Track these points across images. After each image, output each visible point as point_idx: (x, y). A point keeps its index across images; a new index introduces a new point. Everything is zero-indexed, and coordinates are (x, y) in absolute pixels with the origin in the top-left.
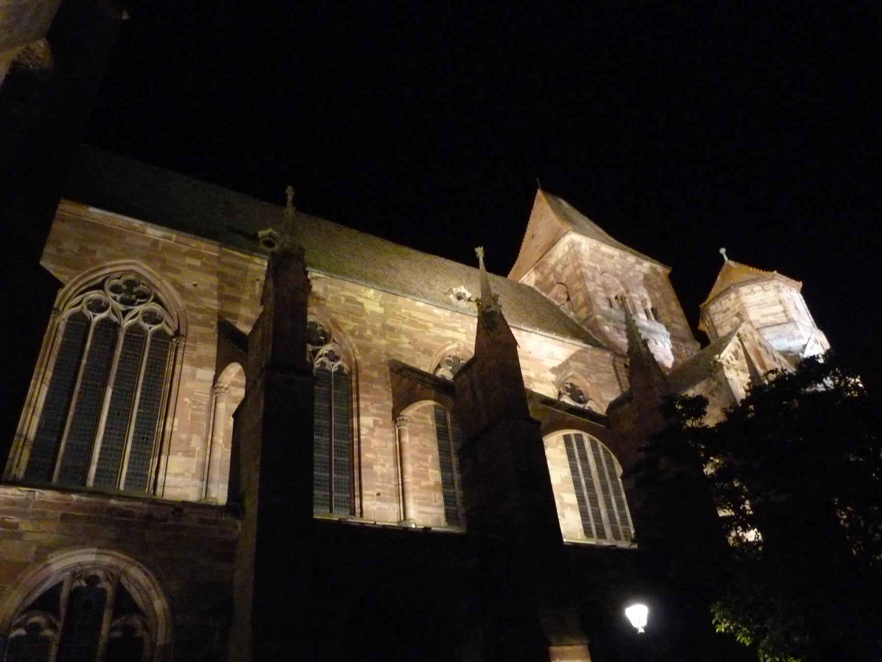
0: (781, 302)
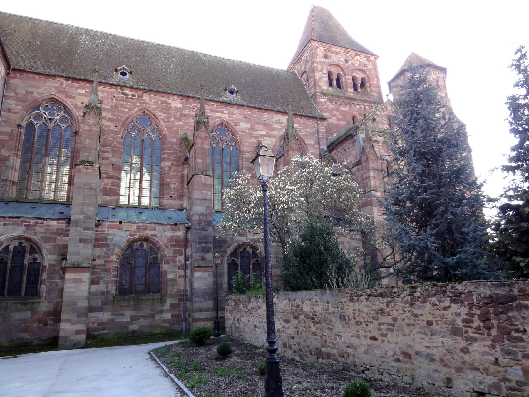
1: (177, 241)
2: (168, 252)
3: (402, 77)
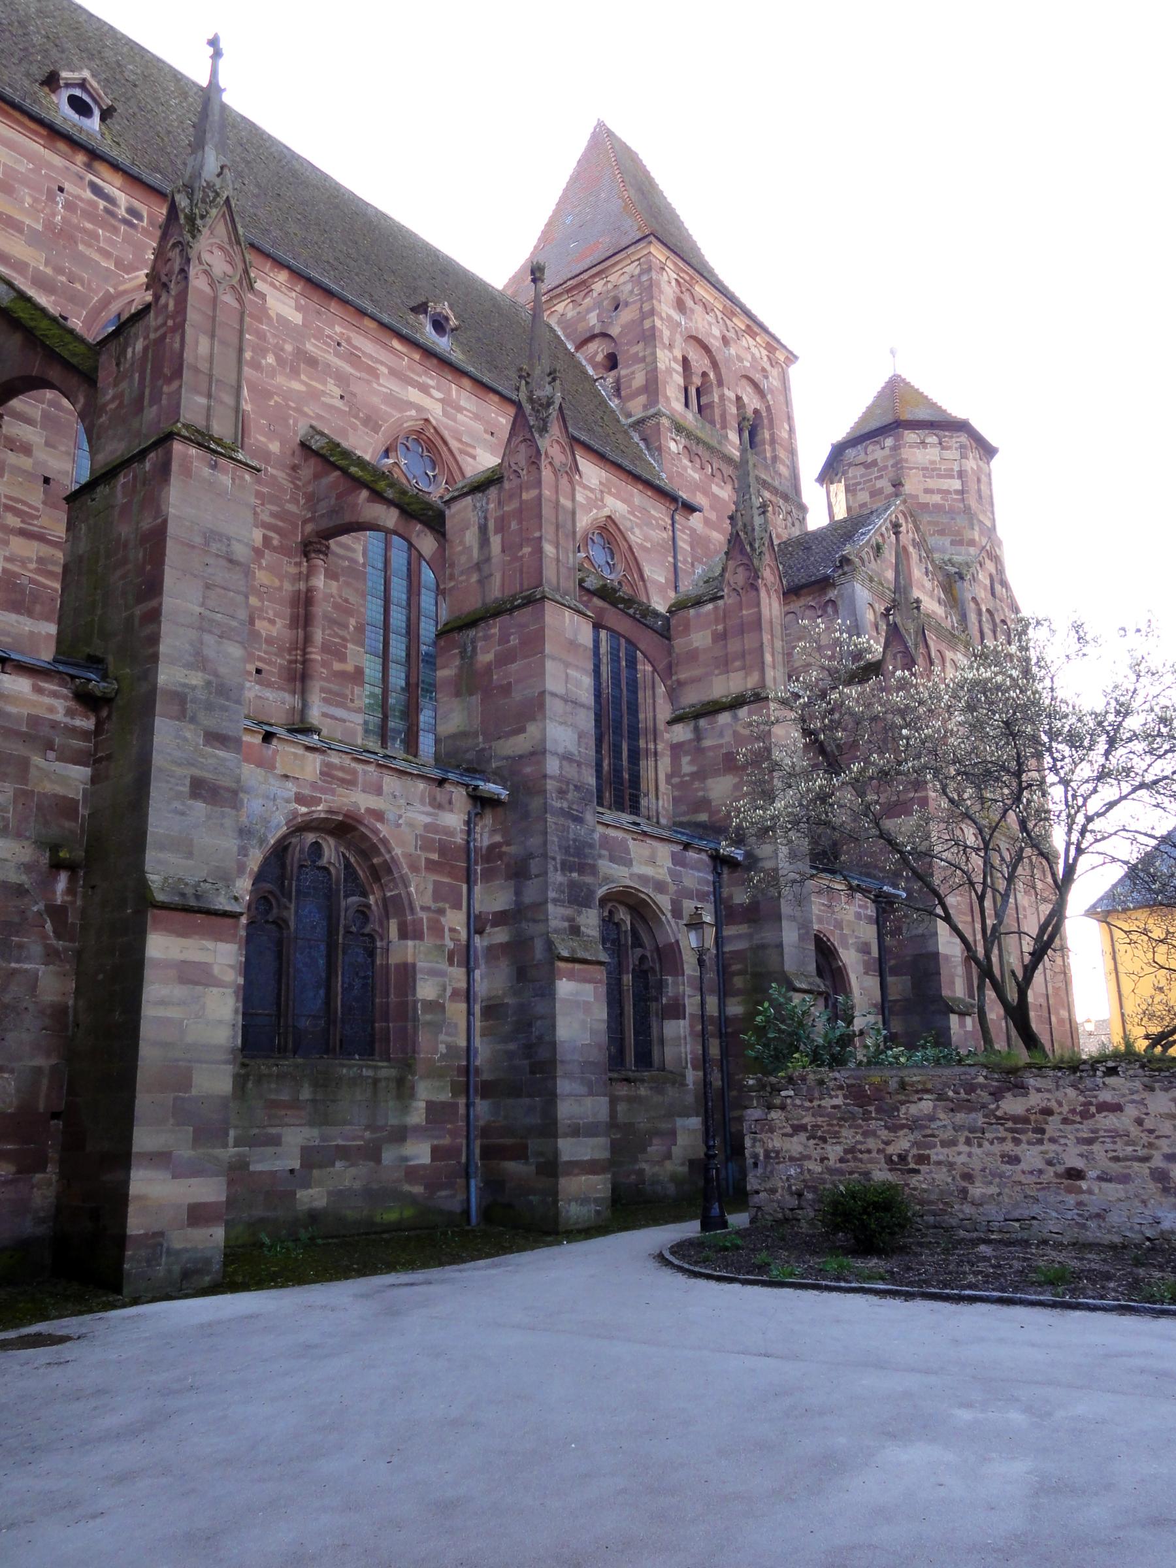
0: (961, 474)
2: (420, 889)
3: (889, 442)
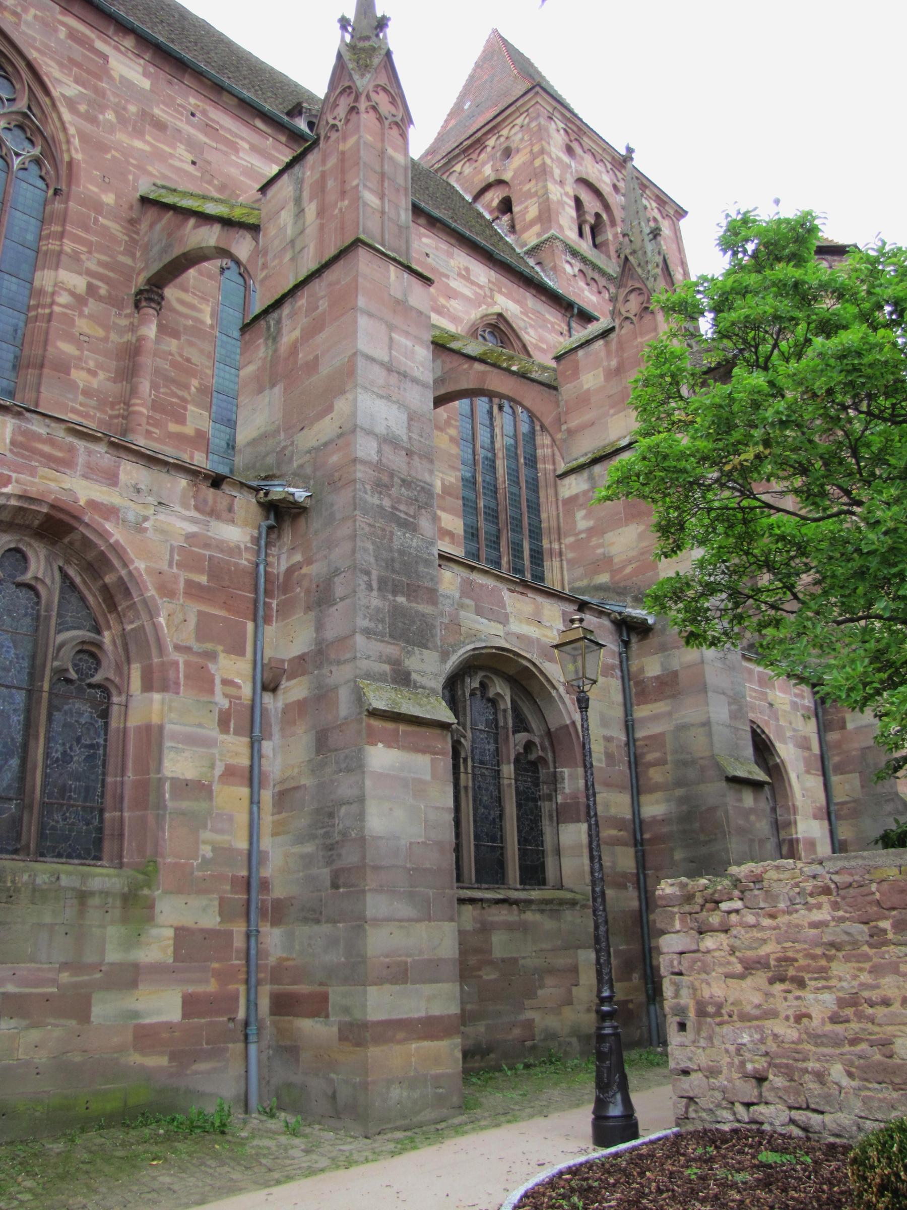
1: (216, 570)
2: (174, 622)
